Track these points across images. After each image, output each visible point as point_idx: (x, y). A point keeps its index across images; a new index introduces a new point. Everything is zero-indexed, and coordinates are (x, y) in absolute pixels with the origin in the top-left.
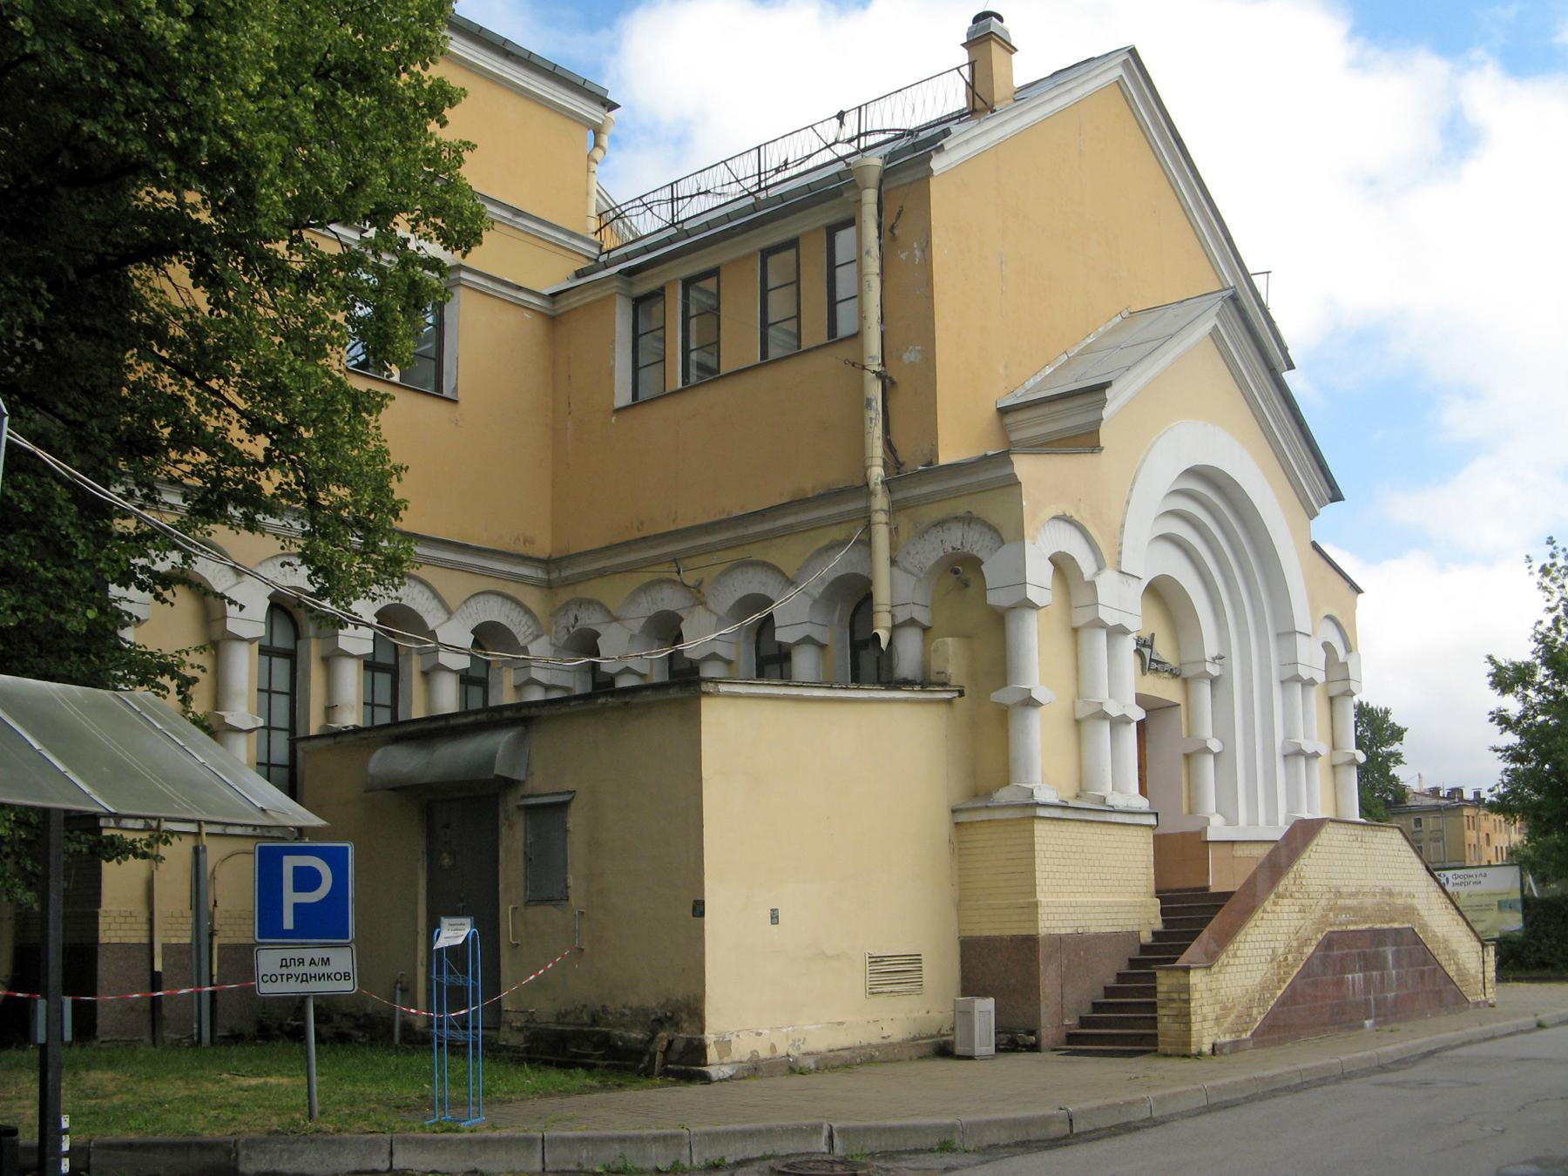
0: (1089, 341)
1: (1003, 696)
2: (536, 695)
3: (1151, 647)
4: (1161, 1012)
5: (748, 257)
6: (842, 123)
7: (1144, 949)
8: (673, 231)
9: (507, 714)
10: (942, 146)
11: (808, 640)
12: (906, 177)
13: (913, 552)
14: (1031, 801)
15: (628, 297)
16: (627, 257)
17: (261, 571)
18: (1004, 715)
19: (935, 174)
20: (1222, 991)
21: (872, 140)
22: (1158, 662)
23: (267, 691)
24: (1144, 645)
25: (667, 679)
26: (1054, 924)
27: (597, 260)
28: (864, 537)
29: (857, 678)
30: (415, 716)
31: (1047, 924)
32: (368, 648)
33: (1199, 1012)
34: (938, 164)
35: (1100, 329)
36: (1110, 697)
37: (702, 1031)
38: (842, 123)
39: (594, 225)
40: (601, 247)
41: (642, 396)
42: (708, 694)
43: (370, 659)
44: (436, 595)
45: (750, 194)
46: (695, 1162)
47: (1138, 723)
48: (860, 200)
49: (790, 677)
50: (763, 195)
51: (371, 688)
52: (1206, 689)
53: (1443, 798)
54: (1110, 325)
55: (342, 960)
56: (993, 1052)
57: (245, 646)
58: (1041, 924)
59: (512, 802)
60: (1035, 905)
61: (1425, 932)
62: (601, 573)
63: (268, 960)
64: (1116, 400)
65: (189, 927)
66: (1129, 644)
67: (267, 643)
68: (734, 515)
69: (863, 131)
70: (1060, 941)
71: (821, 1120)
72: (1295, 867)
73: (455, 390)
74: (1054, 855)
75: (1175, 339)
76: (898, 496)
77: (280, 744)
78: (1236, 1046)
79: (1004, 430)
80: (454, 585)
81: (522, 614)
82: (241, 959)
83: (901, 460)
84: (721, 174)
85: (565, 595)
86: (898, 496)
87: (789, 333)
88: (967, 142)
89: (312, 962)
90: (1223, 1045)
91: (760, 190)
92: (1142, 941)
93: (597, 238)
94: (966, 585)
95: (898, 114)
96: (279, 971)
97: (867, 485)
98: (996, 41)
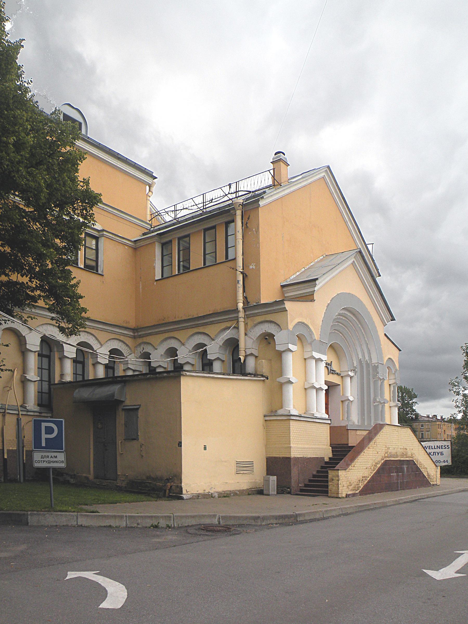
0: (312, 264)
1: (281, 380)
2: (130, 373)
3: (331, 366)
4: (330, 483)
5: (199, 231)
6: (230, 187)
7: (326, 463)
8: (175, 221)
9: (119, 379)
10: (263, 197)
11: (218, 359)
12: (251, 207)
13: (252, 331)
14: (289, 414)
15: (160, 243)
16: (159, 229)
17: (38, 329)
18: (281, 385)
19: (261, 206)
20: (349, 478)
21: (240, 193)
22: (333, 371)
23: (40, 368)
24: (328, 365)
25: (148, 372)
26: (296, 454)
27: (150, 230)
28: (236, 326)
29: (234, 373)
30: (90, 378)
31: (294, 453)
32: (74, 356)
33: (342, 484)
34: (261, 203)
35: (316, 261)
36: (316, 381)
37: (181, 483)
38: (230, 187)
39: (149, 218)
40: (151, 225)
41: (164, 276)
42: (183, 375)
43: (75, 359)
44: (97, 339)
45: (201, 210)
46: (175, 525)
47: (325, 390)
48: (236, 214)
49: (212, 371)
50: (205, 210)
51: (75, 369)
52: (349, 379)
53: (431, 418)
54: (319, 259)
55: (61, 457)
56: (276, 493)
57: (33, 354)
58: (292, 454)
59: (121, 407)
60: (290, 447)
61: (417, 462)
62: (150, 334)
63: (37, 456)
64: (319, 284)
65: (16, 444)
66: (323, 365)
67: (40, 353)
68: (195, 317)
69: (237, 190)
70: (297, 459)
71: (216, 513)
72: (375, 439)
73: (102, 271)
74: (297, 431)
75: (340, 265)
76: (247, 313)
77: (46, 386)
78: (354, 495)
79: (283, 293)
80: (102, 336)
81: (126, 346)
82: (30, 454)
83: (249, 301)
84: (190, 203)
85: (140, 341)
86: (247, 313)
87: (212, 256)
88: (272, 196)
89: (51, 457)
90: (349, 495)
91: (204, 209)
92: (325, 460)
93: (150, 223)
94: (270, 343)
95: (249, 186)
96: (40, 460)
97: (238, 309)
98: (282, 162)
